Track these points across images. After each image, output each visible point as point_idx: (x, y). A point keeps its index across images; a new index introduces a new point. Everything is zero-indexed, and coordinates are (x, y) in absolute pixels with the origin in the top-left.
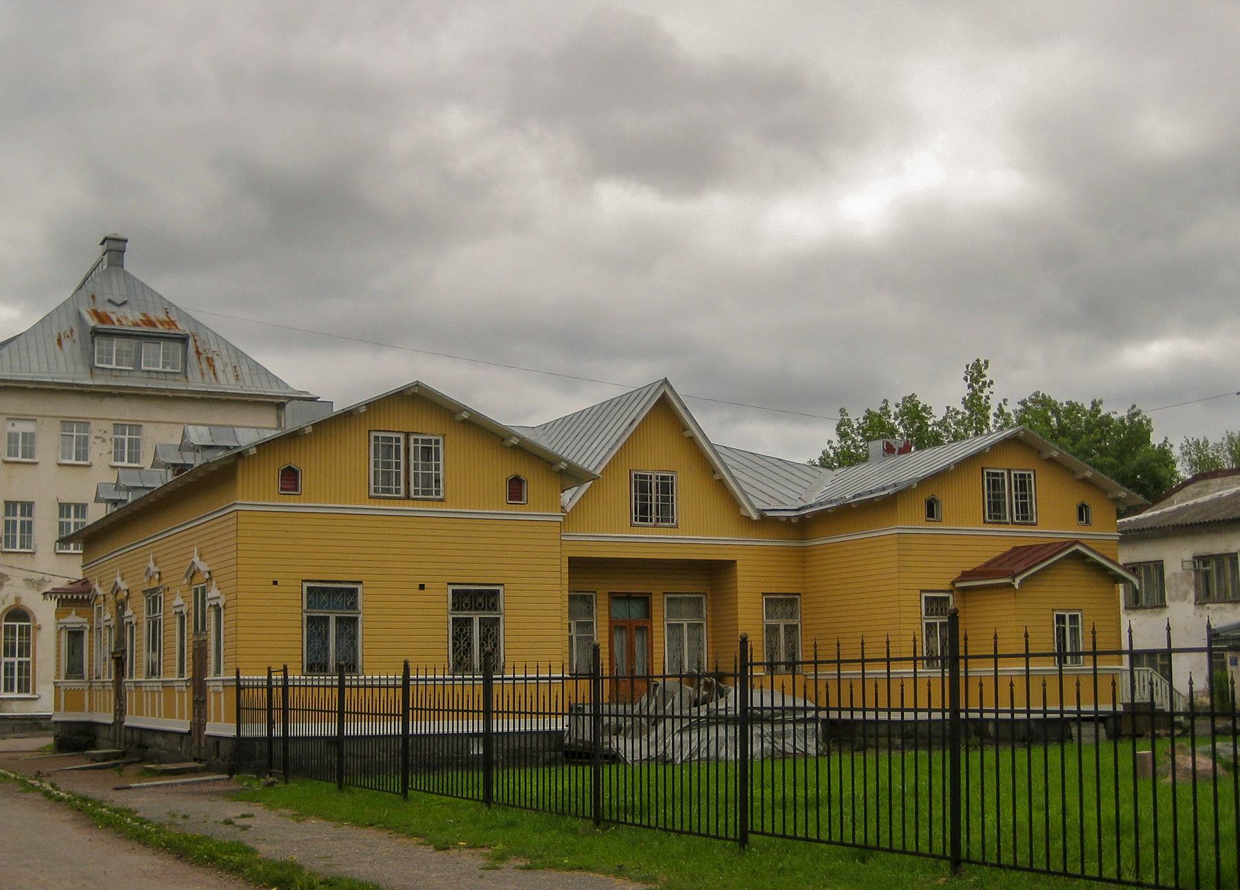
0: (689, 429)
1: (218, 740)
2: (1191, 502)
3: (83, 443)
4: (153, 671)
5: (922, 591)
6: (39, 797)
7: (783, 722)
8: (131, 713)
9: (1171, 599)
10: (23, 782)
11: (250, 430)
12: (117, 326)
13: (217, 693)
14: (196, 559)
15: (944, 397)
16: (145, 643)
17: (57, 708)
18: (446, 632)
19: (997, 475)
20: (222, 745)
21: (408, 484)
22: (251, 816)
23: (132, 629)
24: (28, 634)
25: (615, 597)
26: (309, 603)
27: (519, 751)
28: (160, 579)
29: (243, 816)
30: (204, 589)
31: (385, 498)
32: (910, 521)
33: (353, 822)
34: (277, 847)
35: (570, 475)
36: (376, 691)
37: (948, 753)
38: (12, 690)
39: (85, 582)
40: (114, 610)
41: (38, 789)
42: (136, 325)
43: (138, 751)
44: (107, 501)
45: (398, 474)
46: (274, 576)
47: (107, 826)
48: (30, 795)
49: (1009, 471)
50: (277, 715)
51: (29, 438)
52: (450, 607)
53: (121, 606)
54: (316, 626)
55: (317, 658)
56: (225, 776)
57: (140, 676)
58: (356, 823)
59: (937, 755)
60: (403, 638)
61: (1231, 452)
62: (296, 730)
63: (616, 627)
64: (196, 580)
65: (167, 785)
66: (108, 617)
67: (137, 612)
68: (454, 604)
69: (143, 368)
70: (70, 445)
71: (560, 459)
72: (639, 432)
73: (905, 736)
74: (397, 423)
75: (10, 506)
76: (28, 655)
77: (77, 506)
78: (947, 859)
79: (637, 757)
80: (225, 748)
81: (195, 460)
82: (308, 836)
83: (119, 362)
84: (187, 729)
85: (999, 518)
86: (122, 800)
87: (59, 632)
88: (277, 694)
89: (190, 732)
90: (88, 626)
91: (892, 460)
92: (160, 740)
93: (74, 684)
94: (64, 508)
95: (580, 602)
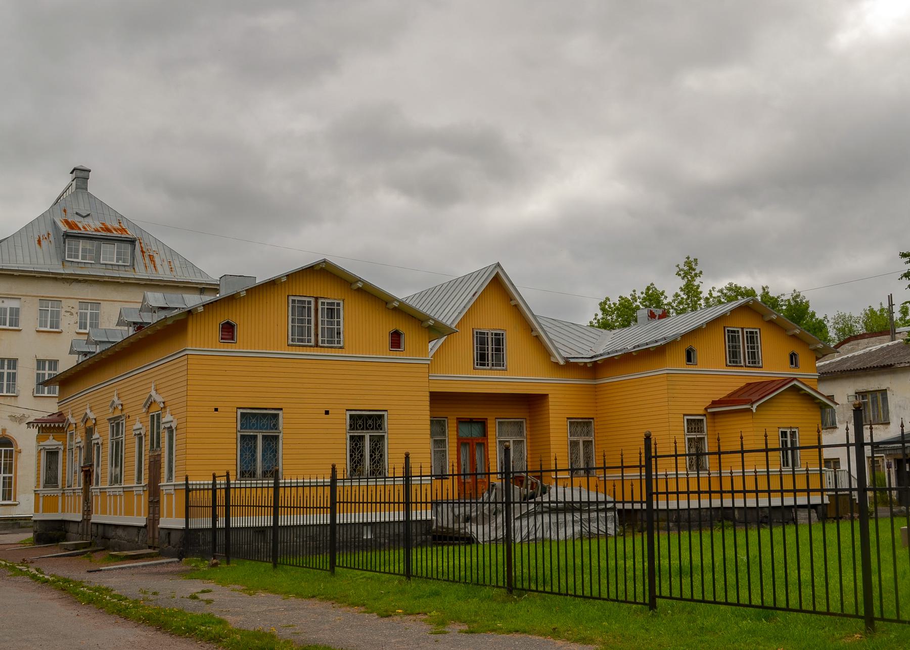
0: (515, 299)
1: (169, 531)
2: (850, 355)
3: (56, 315)
4: (116, 480)
5: (684, 415)
6: (27, 579)
7: (589, 511)
10: (12, 568)
11: (193, 300)
12: (83, 231)
13: (169, 495)
14: (153, 393)
15: (671, 288)
16: (109, 458)
17: (37, 510)
19: (734, 332)
20: (173, 535)
21: (316, 335)
22: (209, 591)
24: (11, 457)
25: (461, 421)
26: (242, 425)
27: (399, 535)
28: (122, 410)
29: (203, 592)
30: (158, 416)
31: (299, 346)
32: (675, 363)
33: (297, 594)
34: (242, 618)
35: (435, 330)
36: (307, 490)
37: (857, 524)
39: (60, 414)
40: (84, 434)
41: (26, 573)
42: (97, 230)
43: (103, 541)
44: (79, 353)
45: (309, 328)
47: (89, 603)
48: (19, 578)
49: (742, 329)
50: (221, 511)
52: (348, 428)
53: (89, 432)
54: (247, 442)
55: (247, 467)
56: (176, 559)
57: (104, 484)
58: (299, 595)
59: (845, 526)
60: (312, 453)
61: (865, 324)
62: (237, 522)
63: (462, 442)
64: (152, 410)
65: (130, 567)
66: (79, 440)
67: (103, 435)
68: (351, 425)
70: (46, 317)
71: (429, 318)
72: (480, 300)
73: (678, 521)
74: (309, 290)
76: (11, 472)
77: (50, 361)
78: (861, 617)
79: (487, 539)
80: (175, 538)
82: (265, 608)
83: (84, 258)
84: (143, 524)
85: (736, 362)
86: (97, 580)
88: (221, 494)
89: (146, 526)
90: (62, 447)
91: (656, 323)
92: (120, 532)
93: (50, 491)
94: (40, 363)
95: (438, 425)
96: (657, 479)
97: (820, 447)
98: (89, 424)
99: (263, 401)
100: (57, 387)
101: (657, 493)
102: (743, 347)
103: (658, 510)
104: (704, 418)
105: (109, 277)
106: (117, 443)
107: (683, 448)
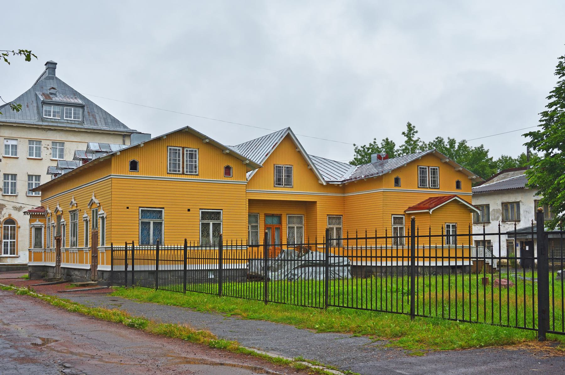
0: (299, 148)
1: (103, 272)
3: (39, 149)
4: (74, 244)
5: (392, 215)
8: (64, 262)
9: (492, 220)
11: (116, 146)
14: (93, 198)
16: (70, 232)
17: (30, 260)
18: (199, 228)
19: (423, 168)
21: (183, 168)
23: (64, 227)
24: (14, 230)
25: (266, 215)
26: (142, 216)
28: (77, 206)
32: (389, 186)
35: (251, 166)
36: (172, 251)
38: (7, 253)
39: (42, 207)
44: (52, 174)
45: (179, 164)
46: (128, 205)
49: (429, 167)
50: (129, 262)
51: (15, 147)
53: (59, 218)
54: (145, 226)
60: (181, 231)
67: (66, 220)
68: (202, 217)
69: (65, 118)
71: (246, 159)
74: (178, 144)
75: (6, 176)
81: (93, 157)
83: (54, 116)
87: (31, 228)
88: (130, 253)
89: (90, 269)
92: (77, 273)
93: (38, 250)
94: (30, 177)
95: (253, 217)
96: (418, 249)
97: (470, 235)
98: (58, 214)
99: (153, 204)
100: (40, 192)
101: (418, 257)
102: (429, 177)
103: (418, 266)
104: (404, 217)
105: (69, 127)
106: (74, 225)
107: (391, 233)
